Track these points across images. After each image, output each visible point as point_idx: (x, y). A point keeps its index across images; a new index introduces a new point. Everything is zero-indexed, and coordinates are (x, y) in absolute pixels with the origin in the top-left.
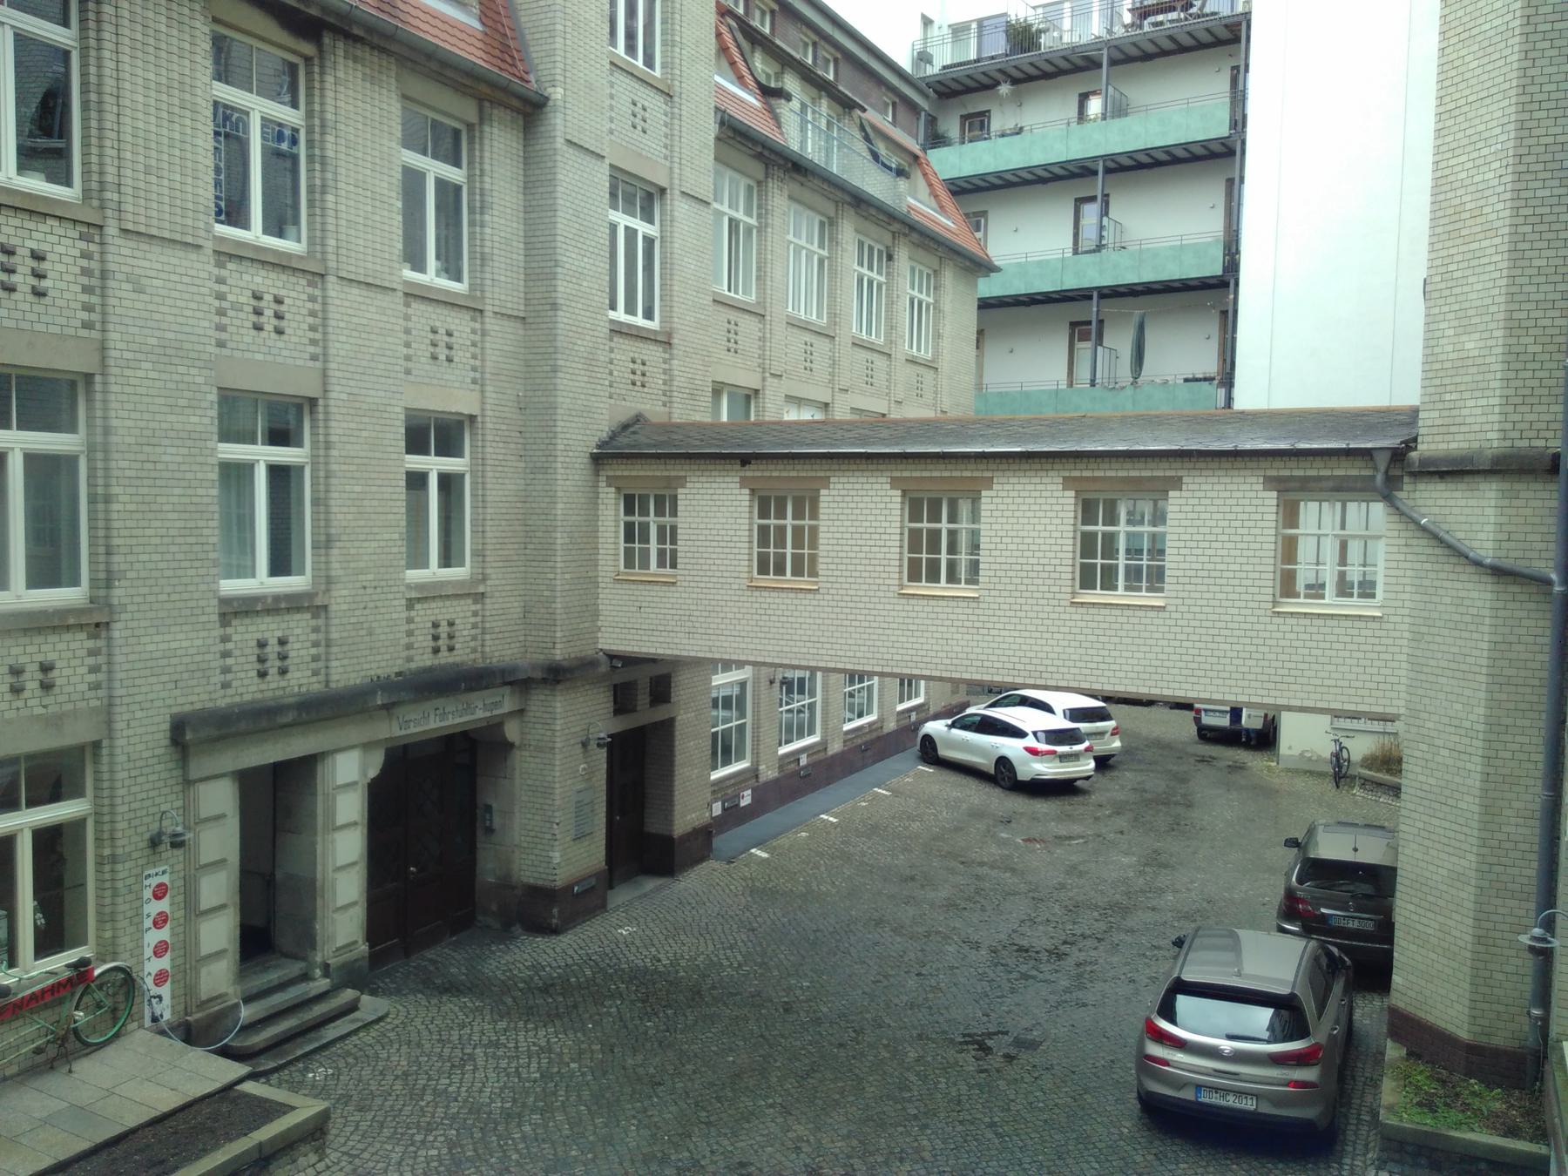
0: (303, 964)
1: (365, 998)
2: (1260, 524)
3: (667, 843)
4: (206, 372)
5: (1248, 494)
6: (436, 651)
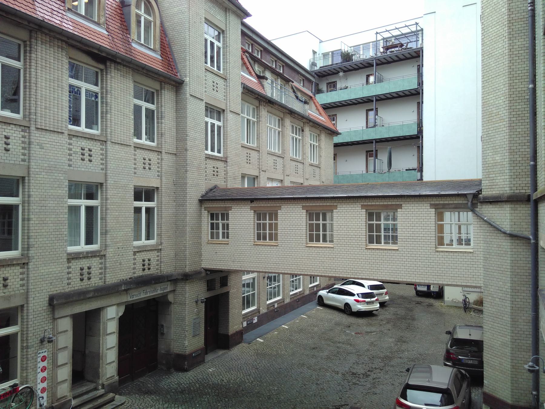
0: (95, 384)
1: (117, 396)
2: (429, 220)
3: (227, 337)
4: (64, 175)
5: (425, 210)
6: (144, 270)
